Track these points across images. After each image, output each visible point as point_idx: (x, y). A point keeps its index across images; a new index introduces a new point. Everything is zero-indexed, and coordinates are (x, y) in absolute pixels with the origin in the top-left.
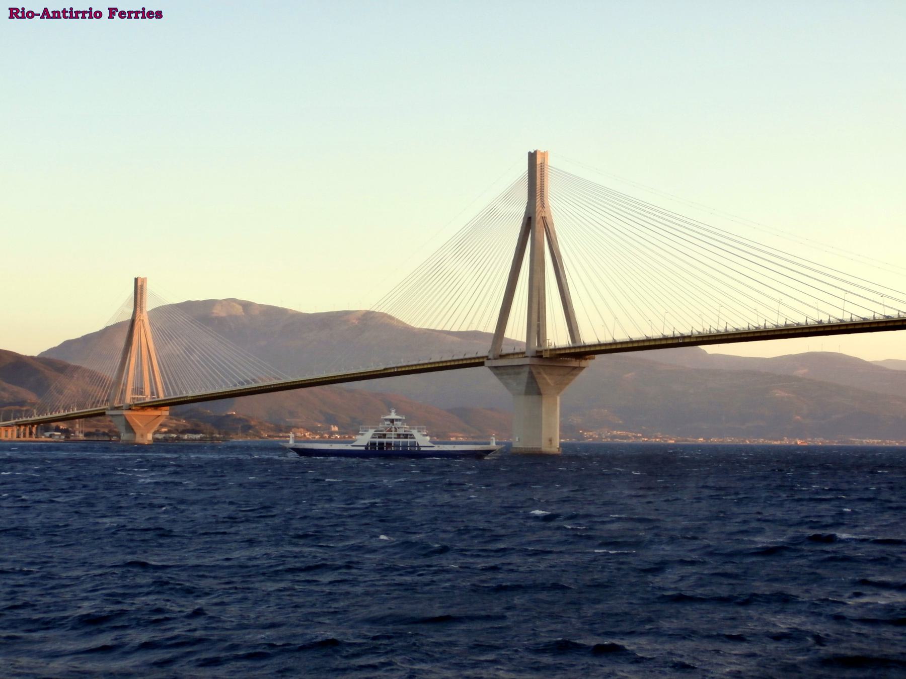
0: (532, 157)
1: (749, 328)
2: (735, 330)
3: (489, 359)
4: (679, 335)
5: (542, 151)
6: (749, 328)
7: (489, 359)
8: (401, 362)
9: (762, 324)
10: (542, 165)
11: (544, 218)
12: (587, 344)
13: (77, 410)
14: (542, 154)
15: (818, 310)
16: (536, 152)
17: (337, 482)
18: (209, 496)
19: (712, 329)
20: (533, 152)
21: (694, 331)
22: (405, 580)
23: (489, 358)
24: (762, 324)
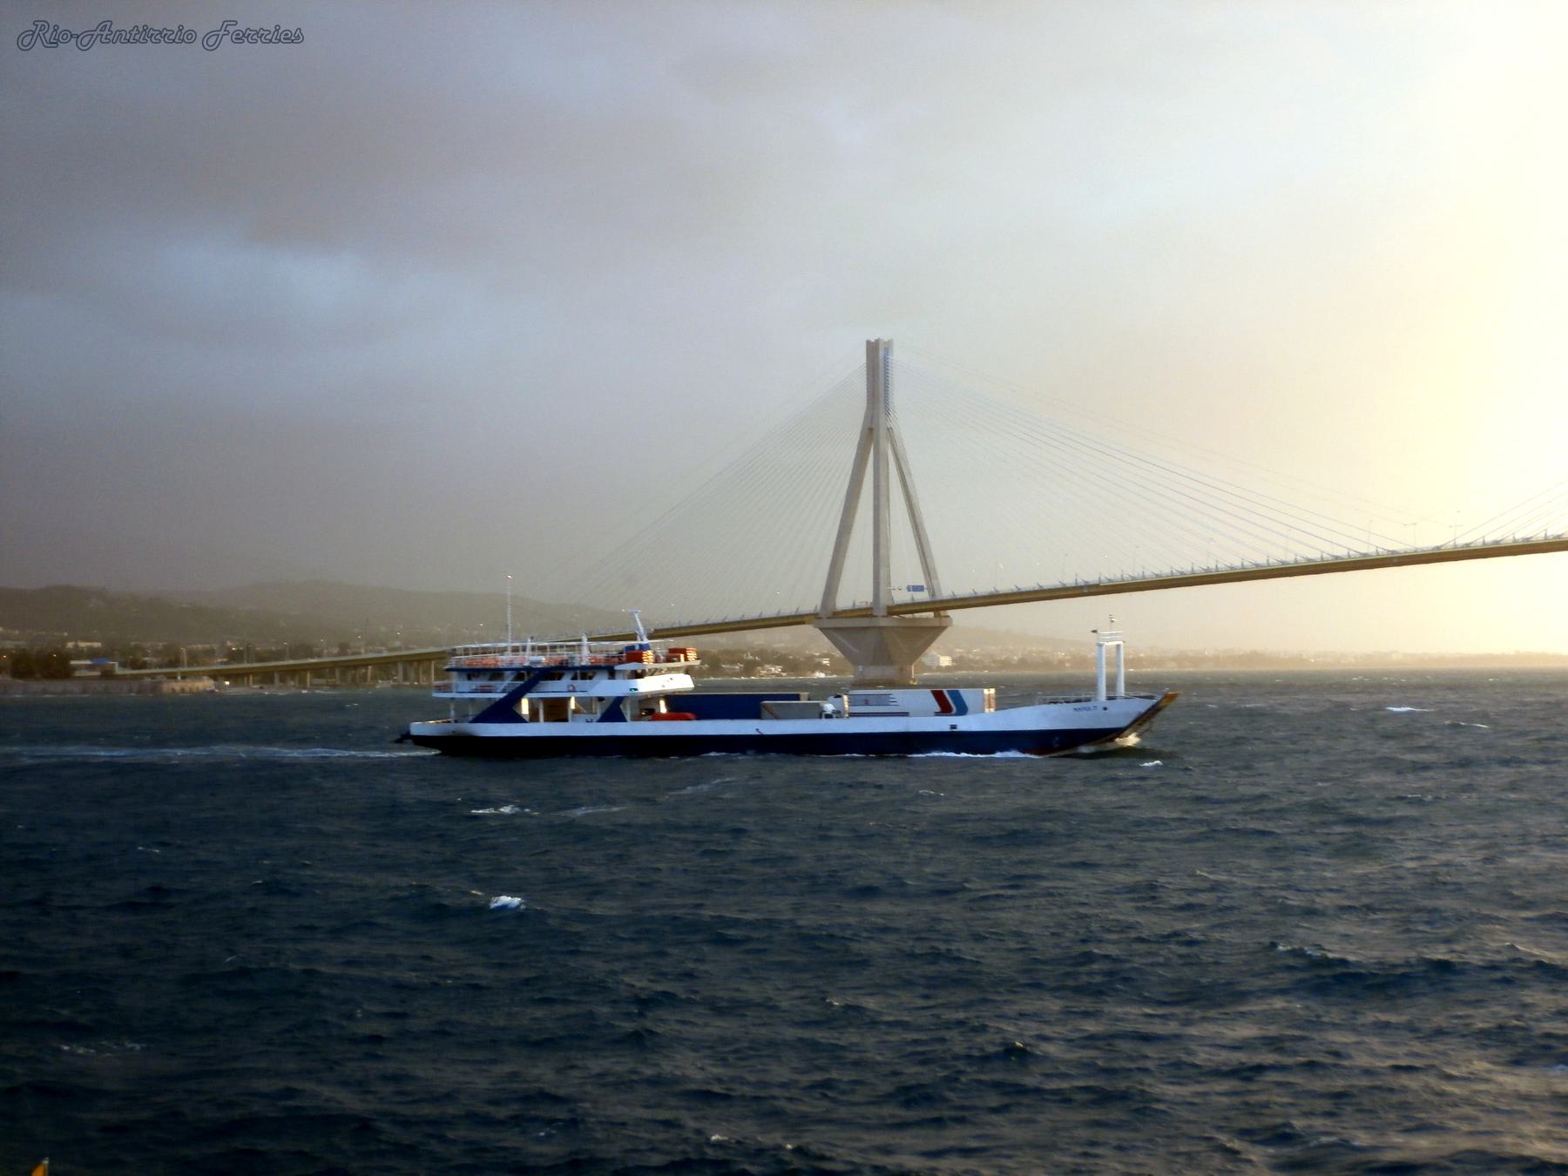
0: (873, 349)
1: (1322, 558)
2: (1229, 569)
3: (820, 618)
4: (1083, 584)
5: (886, 340)
6: (1322, 558)
7: (820, 618)
8: (359, 653)
9: (1213, 566)
11: (889, 430)
12: (958, 597)
13: (436, 680)
14: (885, 343)
15: (1369, 532)
16: (877, 341)
17: (391, 761)
18: (936, 871)
19: (1245, 563)
20: (873, 341)
21: (1103, 578)
22: (1156, 1010)
23: (820, 616)
24: (1119, 576)
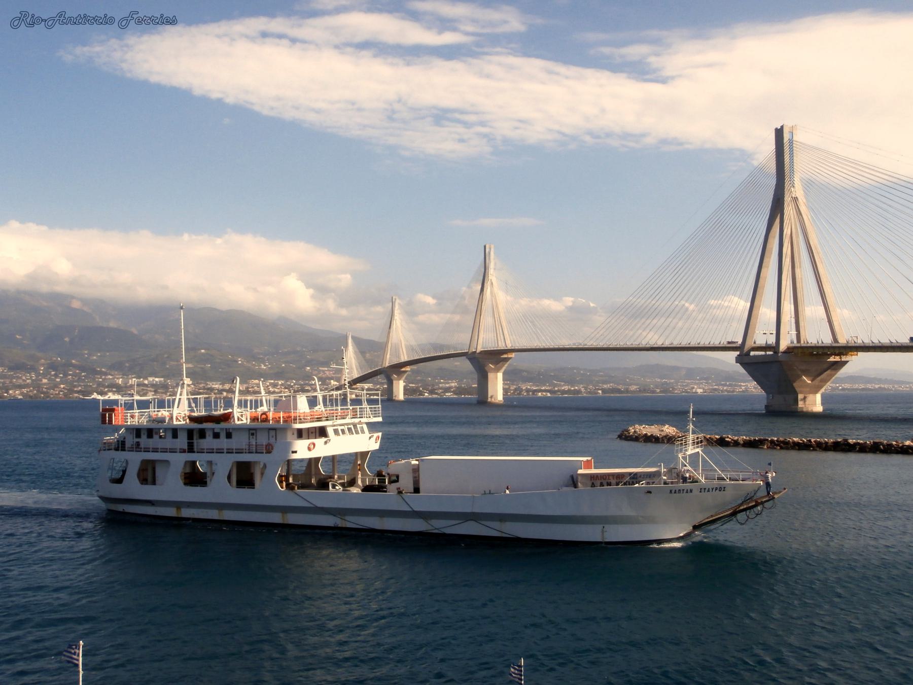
0: (779, 133)
10: (791, 142)
16: (782, 127)
